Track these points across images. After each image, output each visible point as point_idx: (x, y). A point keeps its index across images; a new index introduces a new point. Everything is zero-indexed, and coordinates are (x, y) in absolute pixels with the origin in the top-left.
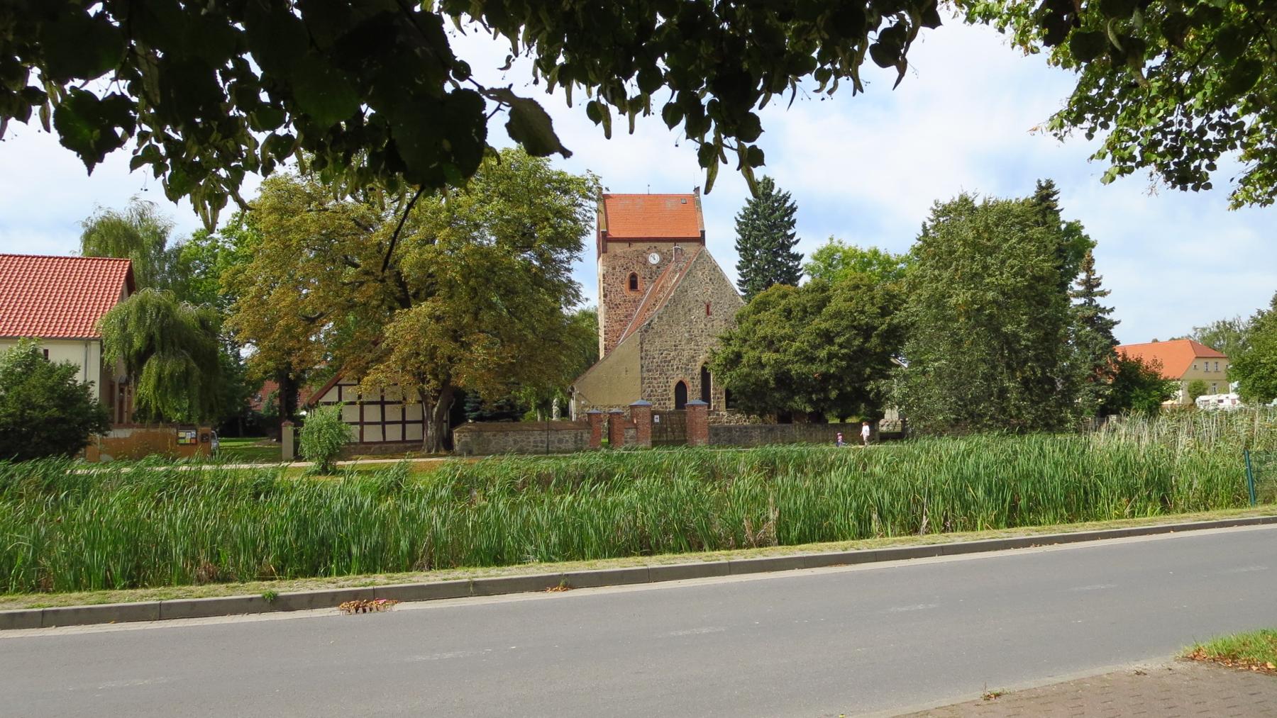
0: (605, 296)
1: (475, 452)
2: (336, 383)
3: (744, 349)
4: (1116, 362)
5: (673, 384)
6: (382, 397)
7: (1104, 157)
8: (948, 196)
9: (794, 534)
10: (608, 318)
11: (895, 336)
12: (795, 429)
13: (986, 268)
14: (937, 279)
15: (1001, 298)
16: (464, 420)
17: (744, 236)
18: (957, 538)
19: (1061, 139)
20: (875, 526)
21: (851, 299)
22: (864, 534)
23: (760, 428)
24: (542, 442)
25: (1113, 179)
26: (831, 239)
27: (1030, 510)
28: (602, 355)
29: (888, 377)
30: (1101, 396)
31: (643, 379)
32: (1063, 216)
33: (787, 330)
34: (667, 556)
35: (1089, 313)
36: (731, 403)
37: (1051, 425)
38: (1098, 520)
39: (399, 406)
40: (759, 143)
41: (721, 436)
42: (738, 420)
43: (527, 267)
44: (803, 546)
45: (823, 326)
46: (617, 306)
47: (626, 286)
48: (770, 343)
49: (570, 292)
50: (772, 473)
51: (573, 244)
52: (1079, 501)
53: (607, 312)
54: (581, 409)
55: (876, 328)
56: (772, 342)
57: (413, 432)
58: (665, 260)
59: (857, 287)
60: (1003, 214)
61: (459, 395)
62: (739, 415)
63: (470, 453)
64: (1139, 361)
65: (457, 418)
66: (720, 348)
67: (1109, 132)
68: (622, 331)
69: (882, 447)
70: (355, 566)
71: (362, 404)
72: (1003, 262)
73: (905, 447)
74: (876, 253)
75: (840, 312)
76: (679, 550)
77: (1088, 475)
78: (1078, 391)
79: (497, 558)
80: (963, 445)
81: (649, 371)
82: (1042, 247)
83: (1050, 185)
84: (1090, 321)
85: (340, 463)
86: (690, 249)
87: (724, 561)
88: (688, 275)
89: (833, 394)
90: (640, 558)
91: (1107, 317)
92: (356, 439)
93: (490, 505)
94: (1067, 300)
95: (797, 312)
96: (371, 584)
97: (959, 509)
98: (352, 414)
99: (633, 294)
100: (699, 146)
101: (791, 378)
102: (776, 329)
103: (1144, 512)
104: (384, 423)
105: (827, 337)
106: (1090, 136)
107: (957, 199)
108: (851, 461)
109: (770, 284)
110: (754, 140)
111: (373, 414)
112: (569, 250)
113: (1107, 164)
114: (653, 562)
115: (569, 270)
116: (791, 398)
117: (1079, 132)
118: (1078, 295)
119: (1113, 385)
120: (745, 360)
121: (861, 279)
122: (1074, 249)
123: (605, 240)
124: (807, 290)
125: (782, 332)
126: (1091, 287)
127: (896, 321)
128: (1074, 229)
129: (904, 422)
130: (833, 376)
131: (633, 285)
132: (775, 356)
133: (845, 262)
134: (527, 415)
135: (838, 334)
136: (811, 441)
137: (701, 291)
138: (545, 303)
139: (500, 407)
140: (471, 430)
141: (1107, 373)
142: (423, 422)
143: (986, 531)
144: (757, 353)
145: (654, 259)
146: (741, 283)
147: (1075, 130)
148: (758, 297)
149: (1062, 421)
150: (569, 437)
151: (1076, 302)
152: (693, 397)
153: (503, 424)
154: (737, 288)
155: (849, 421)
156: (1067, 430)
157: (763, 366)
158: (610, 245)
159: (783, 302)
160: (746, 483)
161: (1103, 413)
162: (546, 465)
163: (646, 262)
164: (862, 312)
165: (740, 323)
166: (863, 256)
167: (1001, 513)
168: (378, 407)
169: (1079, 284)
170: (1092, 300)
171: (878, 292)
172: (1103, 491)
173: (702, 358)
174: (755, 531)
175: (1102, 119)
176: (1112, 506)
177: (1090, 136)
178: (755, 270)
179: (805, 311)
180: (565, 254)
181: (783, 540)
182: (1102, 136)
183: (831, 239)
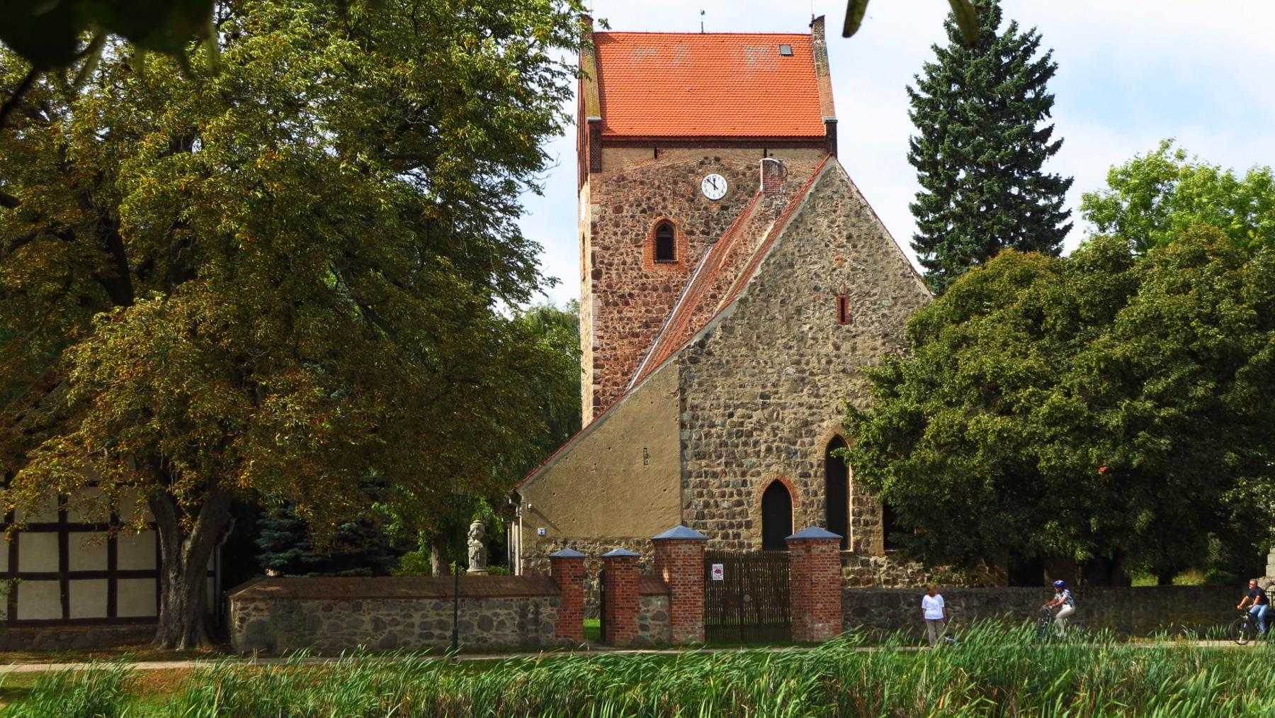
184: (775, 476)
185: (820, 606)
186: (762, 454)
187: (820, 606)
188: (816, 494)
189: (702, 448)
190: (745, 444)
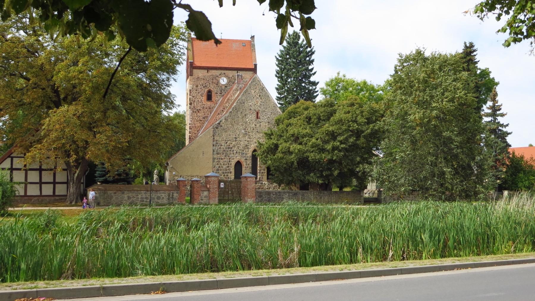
0: (191, 104)
1: (102, 204)
2: (10, 156)
3: (279, 142)
4: (509, 158)
5: (233, 163)
6: (40, 167)
7: (505, 32)
8: (409, 50)
9: (309, 260)
10: (192, 119)
11: (376, 137)
12: (311, 194)
13: (432, 97)
14: (402, 101)
15: (442, 115)
16: (95, 182)
17: (281, 69)
18: (410, 264)
19: (482, 19)
20: (360, 257)
21: (349, 112)
22: (353, 260)
23: (289, 193)
24: (146, 198)
25: (509, 45)
26: (338, 74)
27: (455, 248)
28: (187, 142)
29: (370, 163)
30: (499, 179)
31: (214, 159)
32: (479, 65)
33: (308, 131)
34: (229, 272)
35: (493, 127)
36: (270, 177)
37: (469, 195)
38: (495, 254)
39: (52, 172)
40: (313, 16)
41: (263, 197)
42: (273, 187)
43: (140, 85)
44: (315, 268)
45: (331, 129)
46: (198, 111)
47: (204, 98)
48: (296, 139)
49: (168, 101)
50: (296, 222)
51: (171, 69)
52: (484, 242)
53: (191, 115)
54: (172, 177)
55: (363, 132)
56: (298, 138)
57: (61, 190)
58: (231, 82)
59: (352, 105)
60: (443, 64)
61: (92, 166)
62: (275, 184)
63: (98, 204)
64: (522, 157)
65: (90, 182)
66: (263, 141)
67: (509, 16)
68: (201, 127)
69: (367, 207)
70: (22, 276)
71: (26, 171)
72: (443, 94)
73: (381, 207)
74: (365, 83)
75: (341, 120)
76: (236, 269)
77: (489, 227)
78: (486, 174)
79: (118, 273)
80: (414, 206)
81: (218, 154)
82: (466, 84)
83: (472, 45)
84: (493, 131)
85: (10, 209)
86: (247, 75)
87: (265, 276)
88: (245, 92)
89: (336, 173)
90: (212, 274)
91: (504, 129)
92: (22, 193)
93: (110, 239)
94: (481, 118)
95: (314, 120)
96: (35, 287)
97: (412, 247)
98: (18, 177)
99: (209, 103)
100: (276, 15)
101: (308, 161)
102: (301, 131)
103: (521, 250)
104: (41, 183)
105: (333, 136)
106: (498, 18)
107: (414, 52)
108: (346, 215)
109: (297, 100)
110: (310, 13)
111: (33, 177)
112: (168, 73)
113: (507, 36)
114: (220, 276)
115: (168, 86)
116: (308, 174)
117: (492, 16)
118: (487, 115)
119: (506, 172)
120: (280, 149)
121: (356, 100)
122: (485, 86)
123: (192, 67)
124: (322, 105)
125: (305, 132)
126: (495, 110)
127: (376, 128)
128: (485, 73)
129: (380, 192)
130: (335, 161)
131: (209, 97)
132: (299, 147)
133: (345, 89)
134: (137, 180)
135: (340, 134)
136: (320, 201)
137: (254, 103)
138: (152, 108)
139: (119, 175)
140: (99, 190)
141: (503, 164)
142: (67, 183)
143: (427, 260)
144: (288, 145)
145: (223, 81)
146: (279, 99)
147: (490, 14)
148: (291, 108)
149: (476, 194)
150: (164, 195)
151: (486, 119)
152: (246, 172)
153: (120, 186)
154: (276, 101)
155: (345, 190)
156: (479, 199)
157: (291, 153)
158: (195, 71)
159: (306, 112)
160: (280, 227)
161: (500, 189)
162: (149, 213)
163: (218, 83)
164: (355, 121)
165: (278, 125)
166: (358, 84)
167: (437, 249)
168: (37, 173)
169: (488, 108)
170: (496, 119)
171: (366, 108)
172: (498, 238)
173: (253, 146)
174: (285, 258)
175: (506, 9)
176: (503, 246)
177: (498, 18)
178: (287, 91)
179: (319, 118)
180: (164, 76)
181: (302, 264)
182: (505, 18)
183: (338, 74)
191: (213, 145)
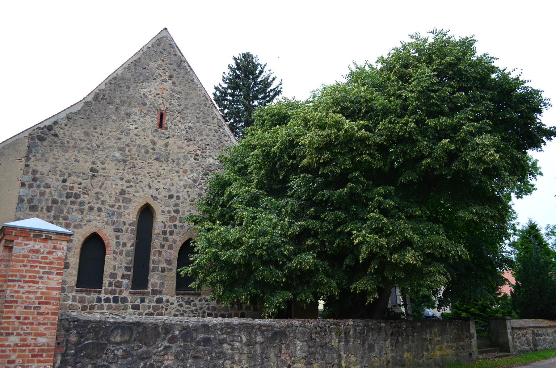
40: (116, 240)
184: (94, 230)
185: (14, 339)
186: (85, 212)
187: (14, 339)
188: (125, 245)
189: (35, 203)
190: (73, 203)
191: (23, 185)
